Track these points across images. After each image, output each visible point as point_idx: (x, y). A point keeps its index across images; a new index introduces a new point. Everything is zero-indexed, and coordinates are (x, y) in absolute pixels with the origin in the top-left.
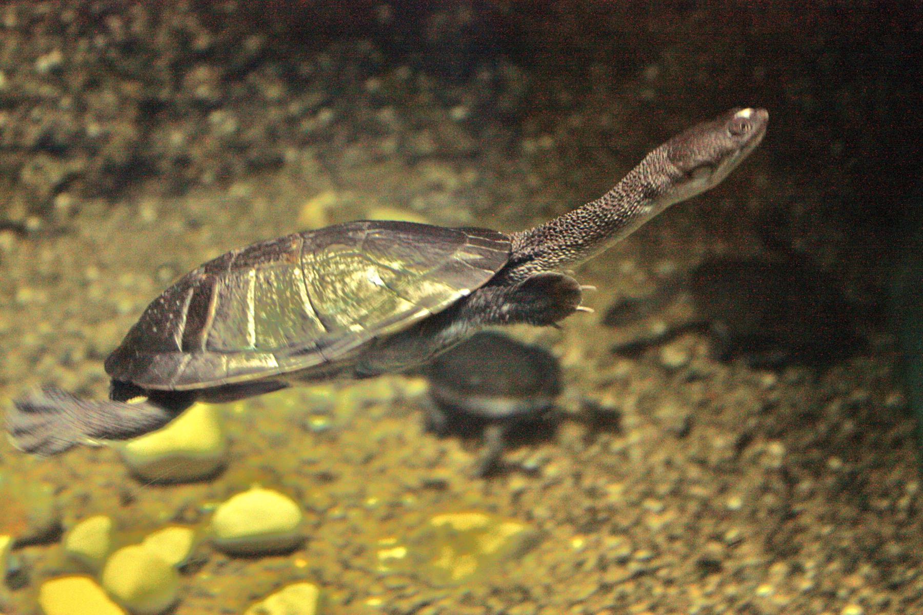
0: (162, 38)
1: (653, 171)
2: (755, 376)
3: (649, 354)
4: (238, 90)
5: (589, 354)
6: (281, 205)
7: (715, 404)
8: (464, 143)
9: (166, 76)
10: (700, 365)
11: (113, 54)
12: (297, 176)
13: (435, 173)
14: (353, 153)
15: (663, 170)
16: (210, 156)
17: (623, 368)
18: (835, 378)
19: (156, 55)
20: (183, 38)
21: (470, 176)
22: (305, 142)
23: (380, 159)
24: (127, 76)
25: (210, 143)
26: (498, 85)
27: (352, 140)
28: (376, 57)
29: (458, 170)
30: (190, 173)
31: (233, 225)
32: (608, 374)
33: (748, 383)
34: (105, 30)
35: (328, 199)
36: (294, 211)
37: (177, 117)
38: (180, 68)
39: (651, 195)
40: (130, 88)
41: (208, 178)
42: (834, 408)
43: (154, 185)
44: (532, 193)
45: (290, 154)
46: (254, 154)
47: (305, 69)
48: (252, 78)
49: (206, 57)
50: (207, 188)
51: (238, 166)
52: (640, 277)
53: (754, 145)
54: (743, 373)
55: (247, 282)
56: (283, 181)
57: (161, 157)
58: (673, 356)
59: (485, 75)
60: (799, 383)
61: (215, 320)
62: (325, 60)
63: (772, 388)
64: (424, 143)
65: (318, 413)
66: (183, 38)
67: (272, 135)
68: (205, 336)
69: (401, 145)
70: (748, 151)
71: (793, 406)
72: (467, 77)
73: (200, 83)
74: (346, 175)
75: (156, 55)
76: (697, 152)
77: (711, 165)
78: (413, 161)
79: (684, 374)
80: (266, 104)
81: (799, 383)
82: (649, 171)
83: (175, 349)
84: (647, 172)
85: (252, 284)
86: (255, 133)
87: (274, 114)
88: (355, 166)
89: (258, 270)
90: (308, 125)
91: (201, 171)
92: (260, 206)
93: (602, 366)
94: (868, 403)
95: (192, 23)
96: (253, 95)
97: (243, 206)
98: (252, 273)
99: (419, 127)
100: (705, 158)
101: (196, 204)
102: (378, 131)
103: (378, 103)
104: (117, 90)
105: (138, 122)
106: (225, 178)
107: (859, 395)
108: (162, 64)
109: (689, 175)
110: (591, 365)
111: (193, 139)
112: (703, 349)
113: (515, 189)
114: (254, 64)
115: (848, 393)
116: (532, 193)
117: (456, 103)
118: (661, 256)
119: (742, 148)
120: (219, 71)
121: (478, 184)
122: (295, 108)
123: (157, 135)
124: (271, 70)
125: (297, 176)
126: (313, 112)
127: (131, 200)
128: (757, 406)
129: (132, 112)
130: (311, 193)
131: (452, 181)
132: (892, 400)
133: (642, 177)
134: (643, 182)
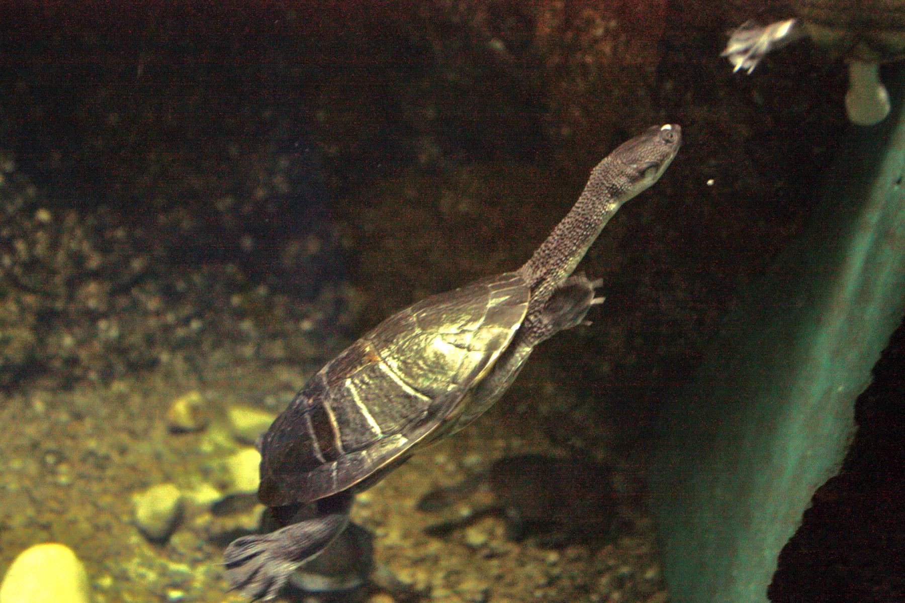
0: (61, 257)
2: (542, 554)
3: (457, 534)
4: (122, 301)
5: (405, 536)
6: (154, 399)
7: (508, 579)
8: (309, 351)
9: (62, 290)
10: (497, 544)
11: (18, 271)
12: (168, 375)
13: (285, 375)
14: (217, 356)
17: (434, 546)
18: (607, 555)
19: (54, 272)
20: (78, 259)
22: (176, 347)
23: (240, 361)
24: (26, 289)
26: (340, 304)
27: (217, 345)
28: (240, 277)
30: (78, 372)
31: (112, 416)
32: (423, 552)
33: (536, 559)
34: (12, 251)
35: (194, 397)
36: (166, 406)
37: (69, 325)
38: (73, 284)
40: (30, 299)
42: (604, 580)
43: (49, 382)
45: (165, 357)
47: (181, 286)
48: (135, 292)
49: (96, 275)
50: (92, 384)
51: (120, 368)
52: (451, 467)
54: (532, 551)
55: (348, 390)
56: (157, 381)
57: (51, 358)
58: (475, 536)
60: (577, 559)
61: (340, 429)
62: (197, 279)
63: (554, 565)
64: (277, 350)
65: (176, 586)
66: (78, 259)
67: (150, 341)
68: (339, 444)
71: (572, 578)
72: (313, 296)
74: (209, 375)
75: (54, 272)
78: (269, 363)
79: (485, 552)
80: (146, 313)
81: (577, 559)
83: (317, 463)
85: (353, 390)
86: (136, 338)
87: (152, 322)
88: (219, 368)
89: (352, 377)
90: (181, 332)
91: (87, 369)
92: (136, 400)
93: (417, 545)
94: (632, 576)
95: (86, 247)
96: (135, 305)
97: (122, 399)
98: (348, 383)
99: (274, 336)
101: (80, 399)
102: (239, 338)
103: (240, 314)
104: (18, 302)
105: (35, 329)
106: (107, 377)
107: (625, 570)
108: (58, 280)
110: (407, 544)
111: (80, 343)
112: (500, 531)
114: (138, 281)
115: (615, 567)
117: (305, 316)
118: (467, 450)
120: (107, 286)
122: (170, 318)
123: (52, 340)
124: (151, 286)
125: (168, 375)
126: (186, 321)
127: (24, 394)
128: (542, 581)
129: (31, 319)
130: (180, 391)
132: (650, 574)
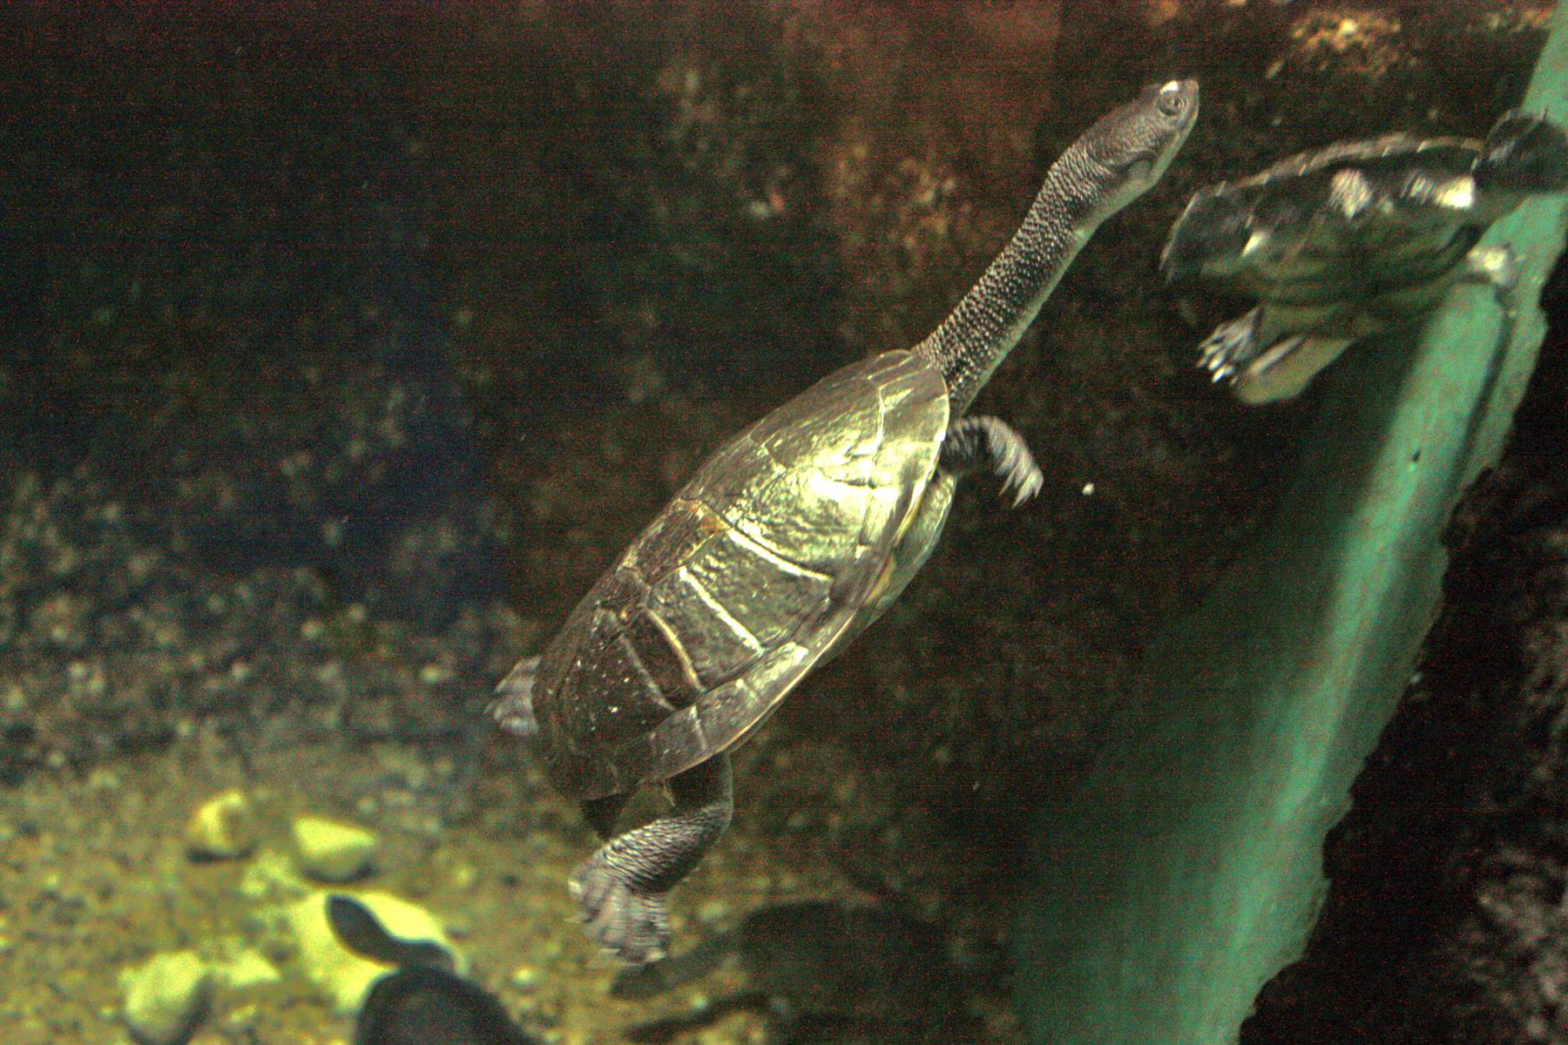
1: (1075, 180)
4: (111, 628)
6: (161, 801)
8: (438, 720)
12: (190, 759)
13: (393, 760)
14: (277, 726)
15: (1088, 174)
16: (63, 727)
21: (445, 767)
23: (314, 738)
25: (66, 708)
27: (274, 709)
28: (318, 591)
29: (428, 758)
30: (31, 752)
31: (89, 829)
39: (1079, 210)
41: (57, 759)
44: (531, 794)
45: (184, 728)
46: (130, 725)
49: (70, 584)
53: (1191, 124)
56: (170, 767)
59: (469, 622)
62: (244, 591)
64: (380, 717)
69: (346, 717)
70: (1187, 132)
72: (443, 625)
73: (59, 621)
74: (261, 761)
76: (1129, 143)
77: (1149, 158)
78: (363, 741)
82: (1069, 181)
84: (1068, 184)
87: (165, 667)
88: (282, 746)
91: (46, 749)
96: (134, 639)
100: (1141, 149)
102: (316, 696)
103: (318, 655)
106: (80, 765)
109: (1123, 173)
113: (506, 785)
114: (138, 596)
116: (531, 794)
119: (1183, 128)
120: (86, 604)
121: (456, 777)
122: (196, 660)
124: (164, 606)
125: (190, 759)
130: (212, 788)
131: (417, 774)
133: (1062, 193)
134: (1066, 199)
